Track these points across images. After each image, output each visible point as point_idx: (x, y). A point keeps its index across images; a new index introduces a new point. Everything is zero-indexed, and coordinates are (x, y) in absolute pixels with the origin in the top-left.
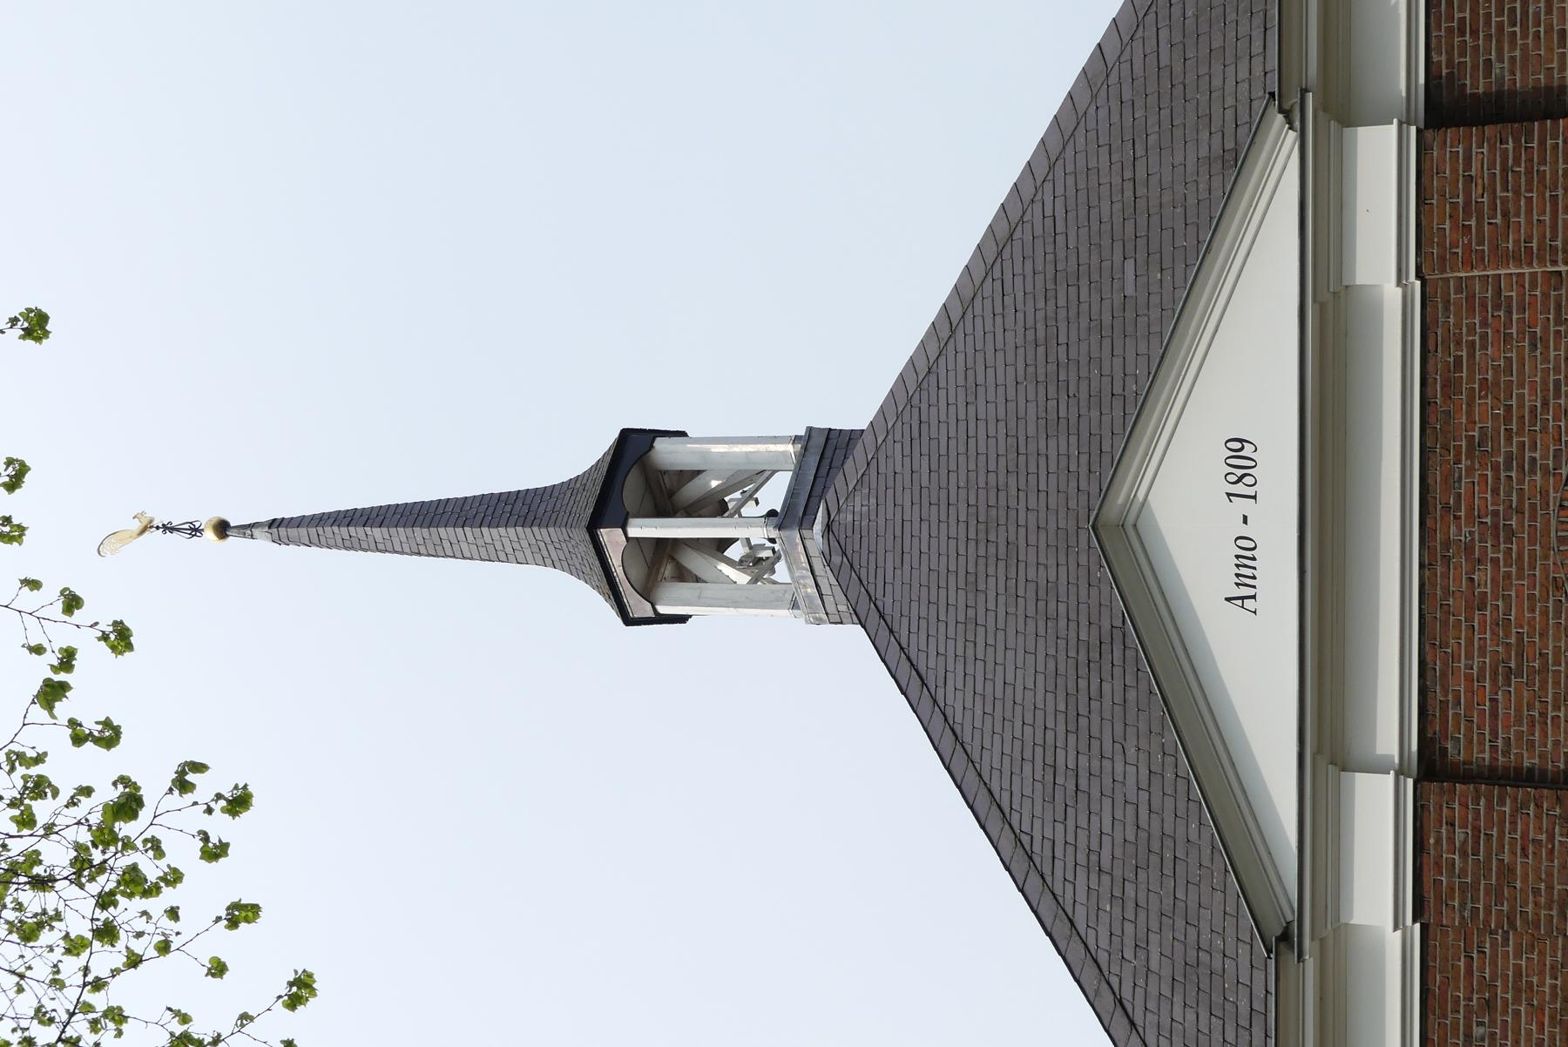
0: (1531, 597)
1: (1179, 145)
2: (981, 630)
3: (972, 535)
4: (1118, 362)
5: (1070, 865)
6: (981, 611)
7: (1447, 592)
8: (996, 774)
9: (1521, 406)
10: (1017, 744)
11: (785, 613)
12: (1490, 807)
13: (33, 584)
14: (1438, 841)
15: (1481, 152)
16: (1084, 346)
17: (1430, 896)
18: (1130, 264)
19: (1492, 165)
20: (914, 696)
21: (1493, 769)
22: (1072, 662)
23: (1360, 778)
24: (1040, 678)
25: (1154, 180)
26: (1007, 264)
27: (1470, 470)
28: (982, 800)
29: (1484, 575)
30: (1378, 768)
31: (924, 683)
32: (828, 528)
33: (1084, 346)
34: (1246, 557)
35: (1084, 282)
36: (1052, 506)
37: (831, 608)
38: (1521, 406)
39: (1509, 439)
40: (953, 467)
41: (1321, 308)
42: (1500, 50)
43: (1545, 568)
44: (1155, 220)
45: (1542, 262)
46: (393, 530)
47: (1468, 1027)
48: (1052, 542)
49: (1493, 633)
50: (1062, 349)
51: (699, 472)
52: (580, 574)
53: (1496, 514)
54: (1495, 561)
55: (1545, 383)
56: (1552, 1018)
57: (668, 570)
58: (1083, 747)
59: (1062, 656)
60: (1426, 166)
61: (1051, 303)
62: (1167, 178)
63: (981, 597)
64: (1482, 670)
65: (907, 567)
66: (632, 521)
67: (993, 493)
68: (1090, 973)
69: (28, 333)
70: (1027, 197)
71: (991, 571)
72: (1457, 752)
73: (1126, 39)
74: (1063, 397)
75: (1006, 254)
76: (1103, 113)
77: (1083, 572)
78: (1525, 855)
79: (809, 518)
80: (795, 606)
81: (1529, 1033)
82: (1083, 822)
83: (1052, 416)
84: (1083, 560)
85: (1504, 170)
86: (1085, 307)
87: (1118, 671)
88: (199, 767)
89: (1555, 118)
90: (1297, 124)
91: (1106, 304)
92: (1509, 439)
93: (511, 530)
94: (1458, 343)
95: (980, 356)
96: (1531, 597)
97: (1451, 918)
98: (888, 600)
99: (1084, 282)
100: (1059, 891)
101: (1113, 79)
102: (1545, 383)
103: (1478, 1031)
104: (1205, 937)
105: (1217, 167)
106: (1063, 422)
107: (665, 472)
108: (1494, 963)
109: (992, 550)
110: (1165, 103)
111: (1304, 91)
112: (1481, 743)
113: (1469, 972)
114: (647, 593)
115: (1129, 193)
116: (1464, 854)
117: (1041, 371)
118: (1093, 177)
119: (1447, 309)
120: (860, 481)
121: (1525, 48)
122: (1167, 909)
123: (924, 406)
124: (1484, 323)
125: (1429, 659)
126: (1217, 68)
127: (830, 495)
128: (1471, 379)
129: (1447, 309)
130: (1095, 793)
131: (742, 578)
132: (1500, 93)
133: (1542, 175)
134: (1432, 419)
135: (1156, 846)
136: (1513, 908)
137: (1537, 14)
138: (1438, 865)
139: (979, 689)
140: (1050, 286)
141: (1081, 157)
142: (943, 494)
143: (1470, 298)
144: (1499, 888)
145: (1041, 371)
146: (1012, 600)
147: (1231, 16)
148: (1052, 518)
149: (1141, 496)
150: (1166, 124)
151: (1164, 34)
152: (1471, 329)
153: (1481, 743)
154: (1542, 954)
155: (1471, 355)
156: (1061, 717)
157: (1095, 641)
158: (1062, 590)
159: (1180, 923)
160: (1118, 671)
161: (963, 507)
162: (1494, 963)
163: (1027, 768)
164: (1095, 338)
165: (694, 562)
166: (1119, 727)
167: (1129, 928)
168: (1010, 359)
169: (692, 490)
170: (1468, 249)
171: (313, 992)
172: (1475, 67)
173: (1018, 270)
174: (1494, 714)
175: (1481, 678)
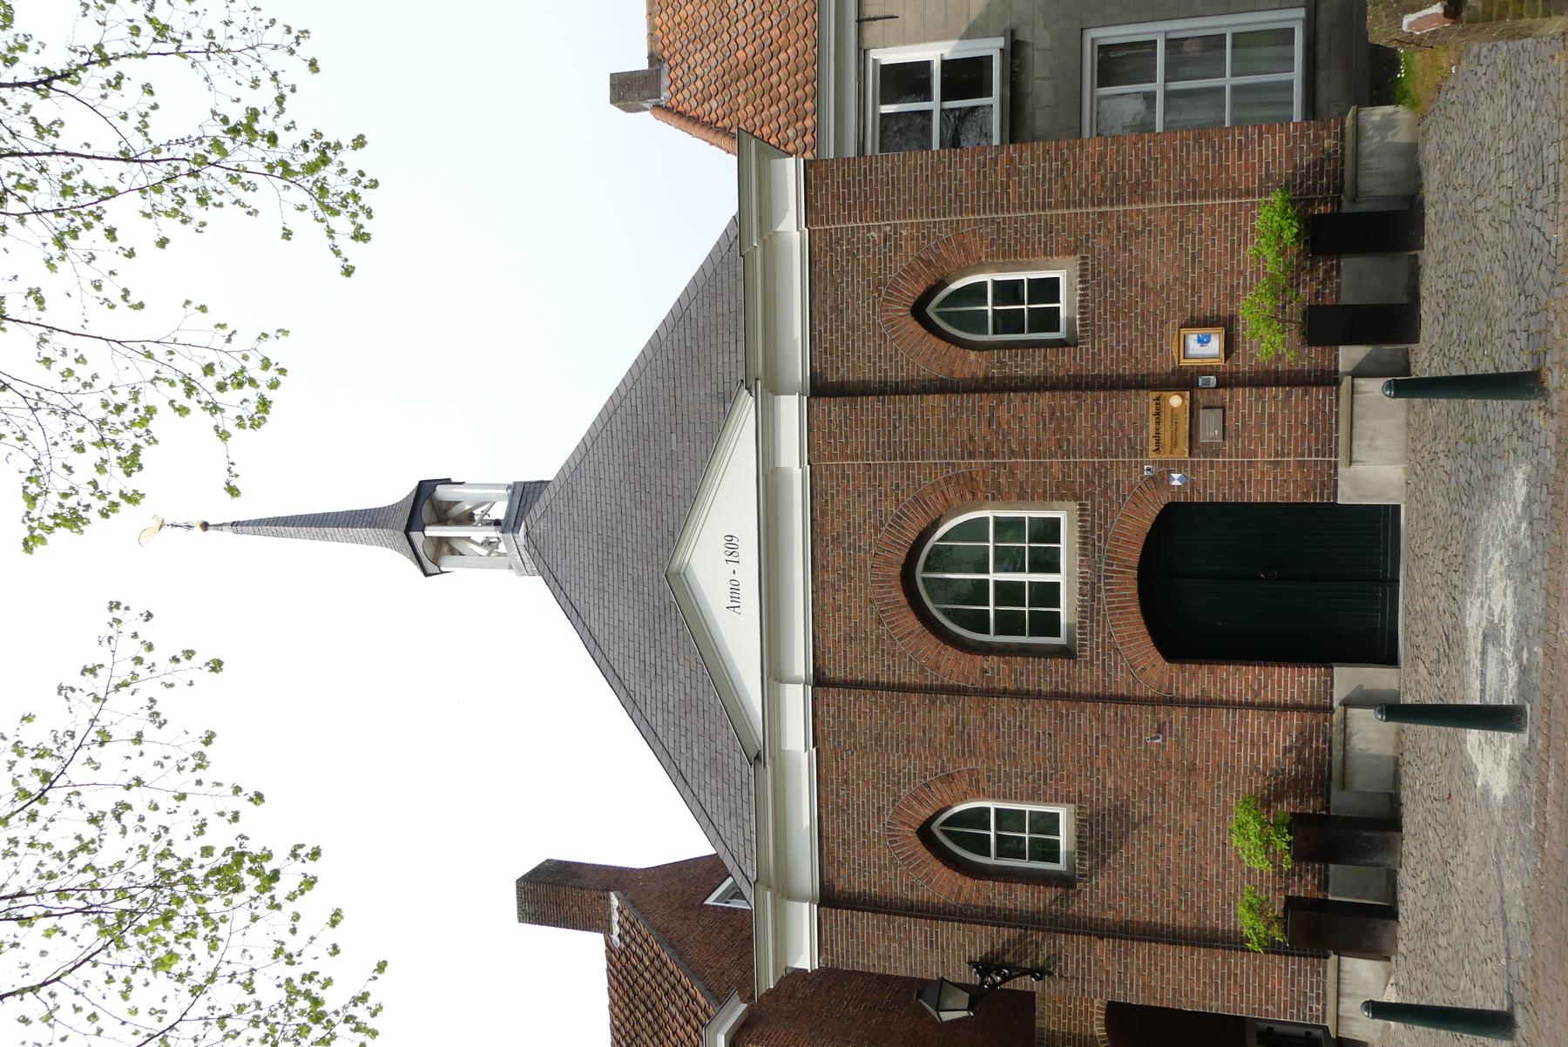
0: (860, 606)
1: (696, 386)
2: (606, 594)
3: (600, 548)
4: (669, 480)
5: (654, 707)
6: (606, 585)
7: (824, 604)
8: (616, 662)
9: (855, 523)
10: (626, 649)
11: (506, 572)
12: (844, 698)
13: (218, 784)
14: (823, 713)
15: (835, 410)
16: (653, 469)
17: (820, 735)
18: (674, 436)
19: (840, 416)
20: (575, 622)
21: (845, 681)
22: (651, 615)
23: (788, 686)
24: (636, 620)
25: (684, 399)
26: (614, 425)
27: (833, 550)
28: (610, 673)
29: (840, 597)
30: (795, 682)
31: (579, 615)
32: (527, 534)
33: (653, 469)
34: (735, 589)
35: (652, 440)
36: (639, 541)
37: (529, 569)
38: (855, 523)
39: (849, 537)
40: (589, 515)
41: (766, 477)
42: (843, 362)
43: (866, 593)
44: (685, 418)
45: (862, 459)
46: (300, 529)
47: (838, 791)
48: (640, 557)
49: (845, 622)
50: (642, 469)
51: (457, 502)
52: (400, 551)
53: (844, 569)
54: (844, 590)
55: (864, 513)
56: (873, 786)
57: (445, 549)
58: (658, 654)
59: (646, 612)
60: (811, 414)
61: (636, 446)
62: (691, 399)
63: (606, 579)
64: (840, 637)
65: (568, 559)
66: (427, 528)
67: (598, 497)
68: (665, 758)
69: (213, 669)
70: (623, 395)
71: (610, 566)
72: (830, 674)
73: (670, 331)
74: (643, 492)
75: (613, 419)
76: (659, 362)
77: (655, 575)
78: (860, 718)
79: (517, 528)
80: (511, 568)
81: (863, 792)
82: (659, 688)
83: (638, 499)
84: (655, 569)
85: (845, 418)
86: (652, 452)
87: (674, 622)
88: (301, 846)
89: (867, 396)
90: (754, 393)
91: (663, 452)
92: (849, 537)
93: (363, 530)
94: (826, 494)
95: (601, 465)
96: (860, 606)
97: (829, 746)
98: (559, 573)
99: (652, 440)
100: (649, 720)
101: (664, 348)
102: (864, 513)
103: (841, 793)
104: (719, 747)
105: (715, 400)
106: (643, 504)
107: (441, 502)
108: (848, 764)
109: (610, 557)
110: (689, 364)
111: (757, 379)
112: (840, 670)
113: (837, 767)
114: (435, 562)
115: (673, 403)
116: (834, 718)
117: (632, 477)
118: (655, 392)
119: (821, 478)
120: (543, 514)
121: (853, 362)
122: (701, 732)
123: (574, 484)
124: (838, 485)
125: (817, 633)
126: (714, 354)
127: (527, 519)
128: (832, 510)
129: (821, 478)
130: (665, 677)
131: (484, 552)
132: (842, 382)
133: (862, 421)
134: (815, 527)
135: (694, 703)
136: (855, 742)
137: (858, 347)
138: (823, 722)
139: (606, 621)
140: (635, 439)
141: (649, 381)
142: (585, 527)
143: (831, 473)
144: (849, 733)
145: (632, 477)
146: (621, 582)
147: (720, 331)
148: (639, 547)
149: (686, 561)
150: (690, 375)
151: (688, 331)
152: (832, 488)
153: (840, 670)
154: (868, 759)
155: (832, 499)
156: (647, 640)
157: (662, 607)
158: (646, 581)
159: (707, 740)
160: (674, 622)
161: (595, 535)
162: (848, 764)
163: (632, 661)
164: (658, 468)
165: (458, 546)
166: (675, 648)
167: (683, 739)
168: (617, 469)
169: (456, 510)
170: (830, 453)
171: (342, 917)
172: (832, 369)
173: (619, 428)
174: (845, 657)
175: (839, 641)
